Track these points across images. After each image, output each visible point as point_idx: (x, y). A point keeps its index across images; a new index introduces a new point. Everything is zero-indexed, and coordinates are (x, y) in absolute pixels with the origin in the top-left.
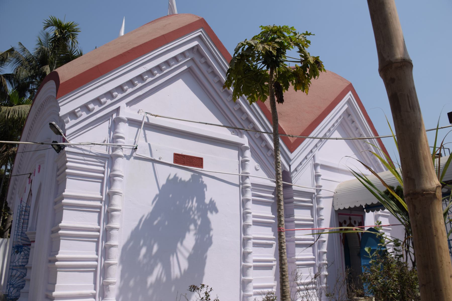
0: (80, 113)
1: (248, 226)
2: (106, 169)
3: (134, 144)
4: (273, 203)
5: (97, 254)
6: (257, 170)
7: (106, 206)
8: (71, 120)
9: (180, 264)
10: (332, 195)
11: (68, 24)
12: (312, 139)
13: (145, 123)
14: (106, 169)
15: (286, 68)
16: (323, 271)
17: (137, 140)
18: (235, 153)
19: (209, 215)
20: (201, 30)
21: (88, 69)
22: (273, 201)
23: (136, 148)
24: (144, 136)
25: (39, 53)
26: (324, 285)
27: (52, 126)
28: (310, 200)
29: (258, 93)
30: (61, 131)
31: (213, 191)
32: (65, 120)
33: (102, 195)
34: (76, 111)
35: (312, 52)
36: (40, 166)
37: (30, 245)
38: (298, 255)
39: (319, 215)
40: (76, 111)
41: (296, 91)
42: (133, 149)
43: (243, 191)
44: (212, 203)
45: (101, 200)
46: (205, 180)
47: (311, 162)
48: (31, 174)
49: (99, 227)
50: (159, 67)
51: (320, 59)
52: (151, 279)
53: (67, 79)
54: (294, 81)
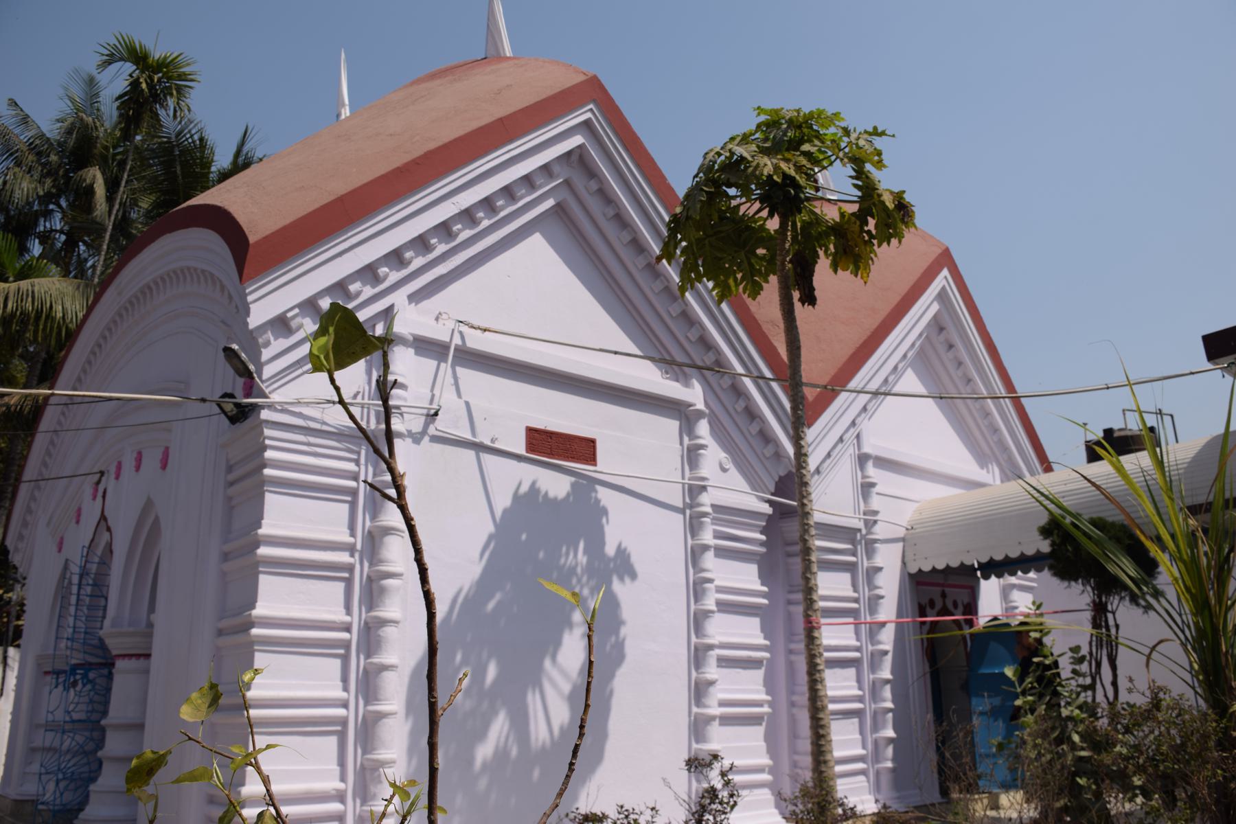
0: (299, 320)
1: (707, 614)
2: (363, 468)
3: (431, 403)
4: (762, 555)
5: (346, 689)
6: (724, 470)
7: (366, 564)
8: (276, 339)
9: (552, 712)
10: (902, 535)
11: (165, 58)
12: (854, 394)
13: (456, 349)
14: (363, 468)
15: (815, 214)
16: (884, 727)
17: (437, 392)
18: (671, 426)
19: (617, 586)
20: (591, 106)
21: (317, 206)
22: (763, 550)
23: (436, 414)
24: (452, 381)
25: (69, 132)
26: (889, 764)
27: (229, 353)
28: (849, 546)
29: (739, 276)
30: (252, 367)
31: (625, 524)
32: (260, 340)
33: (353, 534)
34: (289, 315)
35: (887, 181)
36: (140, 455)
37: (113, 665)
38: (834, 688)
39: (871, 585)
40: (289, 315)
41: (835, 271)
42: (428, 415)
43: (694, 526)
44: (622, 553)
45: (351, 549)
46: (603, 494)
47: (851, 450)
48: (102, 473)
49: (348, 619)
50: (488, 203)
51: (908, 198)
52: (484, 751)
53: (268, 232)
54: (832, 246)
